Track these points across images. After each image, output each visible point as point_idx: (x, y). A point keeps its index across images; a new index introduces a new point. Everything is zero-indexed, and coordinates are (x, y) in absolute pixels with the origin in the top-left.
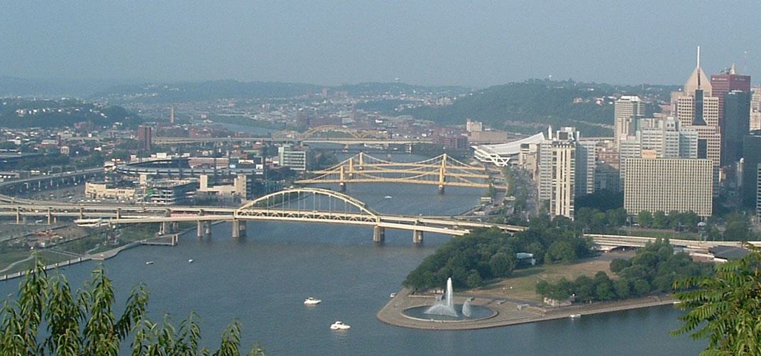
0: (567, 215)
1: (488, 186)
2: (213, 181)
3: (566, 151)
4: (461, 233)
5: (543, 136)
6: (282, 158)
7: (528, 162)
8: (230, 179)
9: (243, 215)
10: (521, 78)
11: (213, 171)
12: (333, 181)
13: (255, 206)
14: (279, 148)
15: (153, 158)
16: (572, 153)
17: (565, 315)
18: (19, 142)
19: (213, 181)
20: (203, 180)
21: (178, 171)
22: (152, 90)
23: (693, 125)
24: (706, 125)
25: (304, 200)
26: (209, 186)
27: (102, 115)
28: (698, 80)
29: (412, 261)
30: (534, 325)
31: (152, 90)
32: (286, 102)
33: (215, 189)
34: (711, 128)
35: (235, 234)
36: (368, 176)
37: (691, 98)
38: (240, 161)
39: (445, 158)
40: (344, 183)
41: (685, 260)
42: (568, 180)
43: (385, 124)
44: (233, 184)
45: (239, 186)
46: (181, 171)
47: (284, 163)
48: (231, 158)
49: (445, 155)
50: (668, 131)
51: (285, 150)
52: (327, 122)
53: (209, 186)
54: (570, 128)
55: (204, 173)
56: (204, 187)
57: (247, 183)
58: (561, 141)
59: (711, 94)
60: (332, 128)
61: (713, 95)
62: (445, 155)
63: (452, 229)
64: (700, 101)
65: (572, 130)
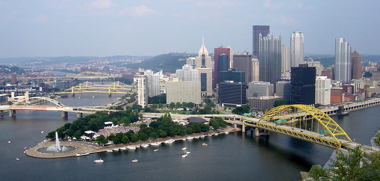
1: (127, 93)
10: (167, 52)
11: (16, 90)
12: (106, 92)
16: (144, 80)
17: (105, 150)
21: (3, 91)
22: (40, 61)
23: (201, 67)
24: (206, 67)
26: (15, 96)
27: (9, 70)
28: (204, 50)
29: (56, 126)
31: (40, 61)
32: (85, 63)
34: (208, 69)
35: (10, 115)
36: (117, 91)
37: (200, 57)
38: (34, 86)
40: (73, 93)
41: (170, 124)
42: (143, 91)
46: (4, 91)
47: (57, 86)
50: (186, 70)
53: (15, 96)
57: (29, 95)
59: (208, 56)
61: (209, 56)
63: (288, 126)
64: (204, 58)
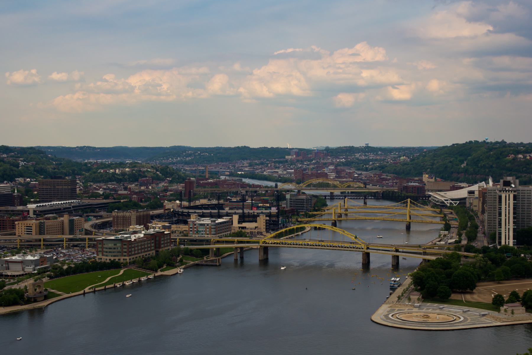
0: (511, 245)
2: (243, 218)
3: (509, 195)
4: (433, 258)
5: (485, 183)
6: (289, 203)
7: (474, 204)
8: (253, 218)
9: (266, 243)
13: (275, 237)
14: (287, 195)
15: (198, 203)
18: (101, 193)
19: (243, 218)
20: (236, 218)
22: (190, 155)
25: (199, 229)
30: (492, 330)
31: (190, 155)
33: (244, 225)
39: (409, 202)
43: (360, 177)
44: (256, 222)
45: (262, 221)
47: (291, 206)
48: (285, 201)
49: (409, 200)
51: (290, 197)
52: (318, 176)
54: (511, 178)
55: (235, 213)
56: (236, 224)
58: (504, 187)
60: (320, 180)
62: (409, 200)
65: (513, 179)
